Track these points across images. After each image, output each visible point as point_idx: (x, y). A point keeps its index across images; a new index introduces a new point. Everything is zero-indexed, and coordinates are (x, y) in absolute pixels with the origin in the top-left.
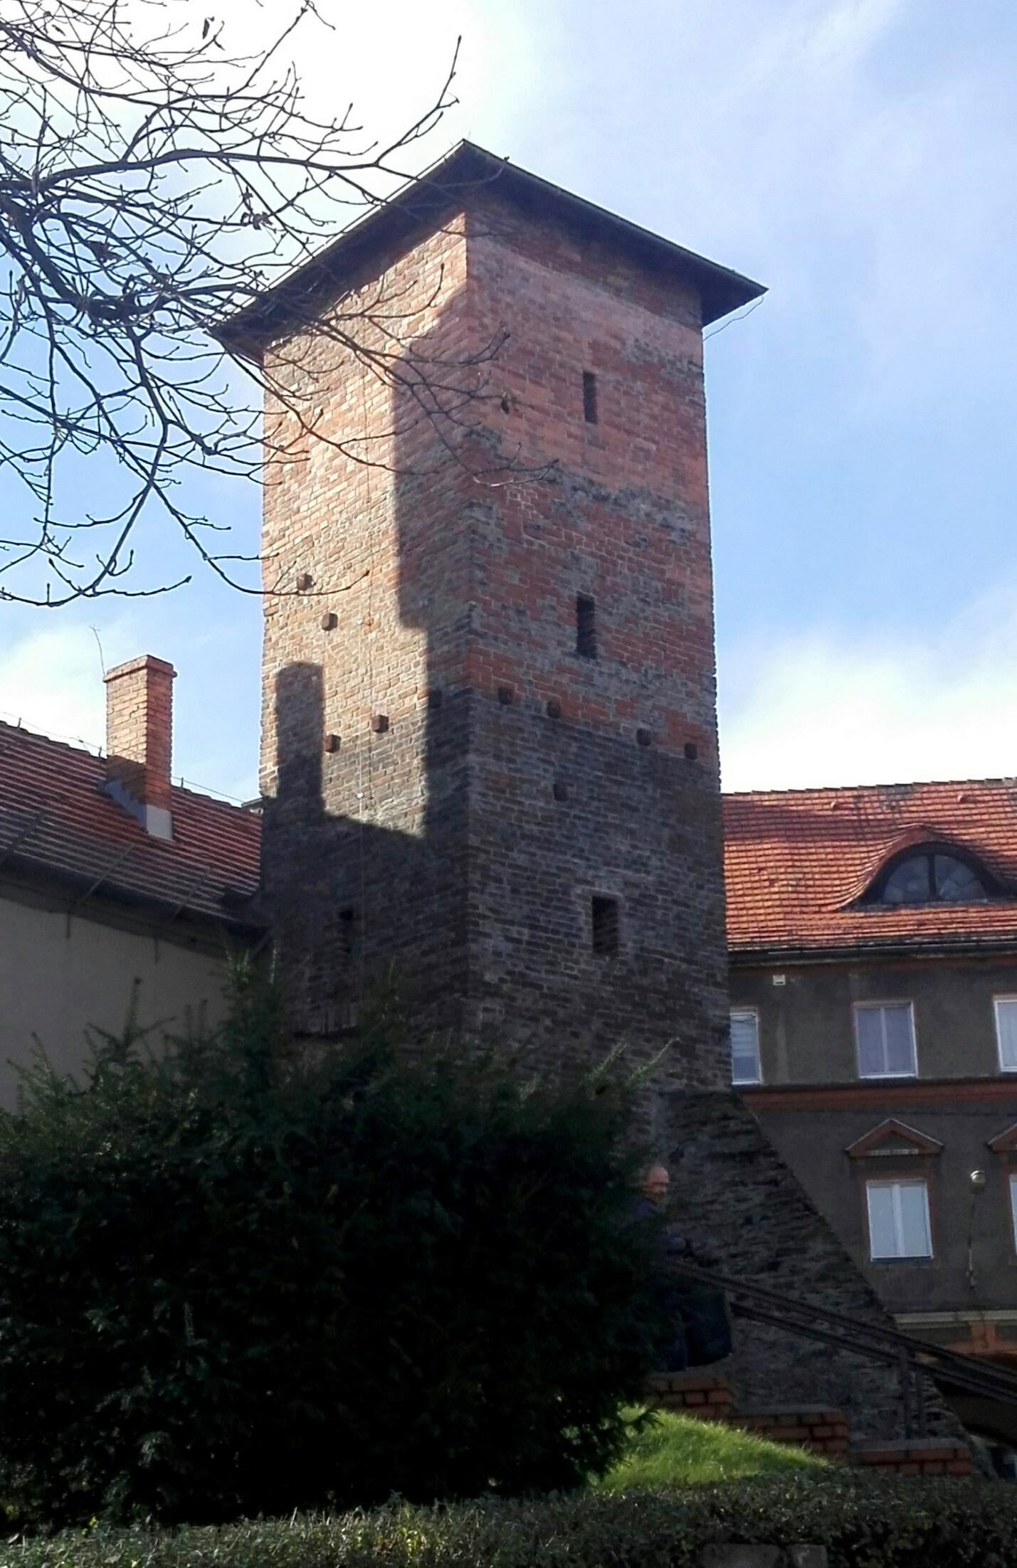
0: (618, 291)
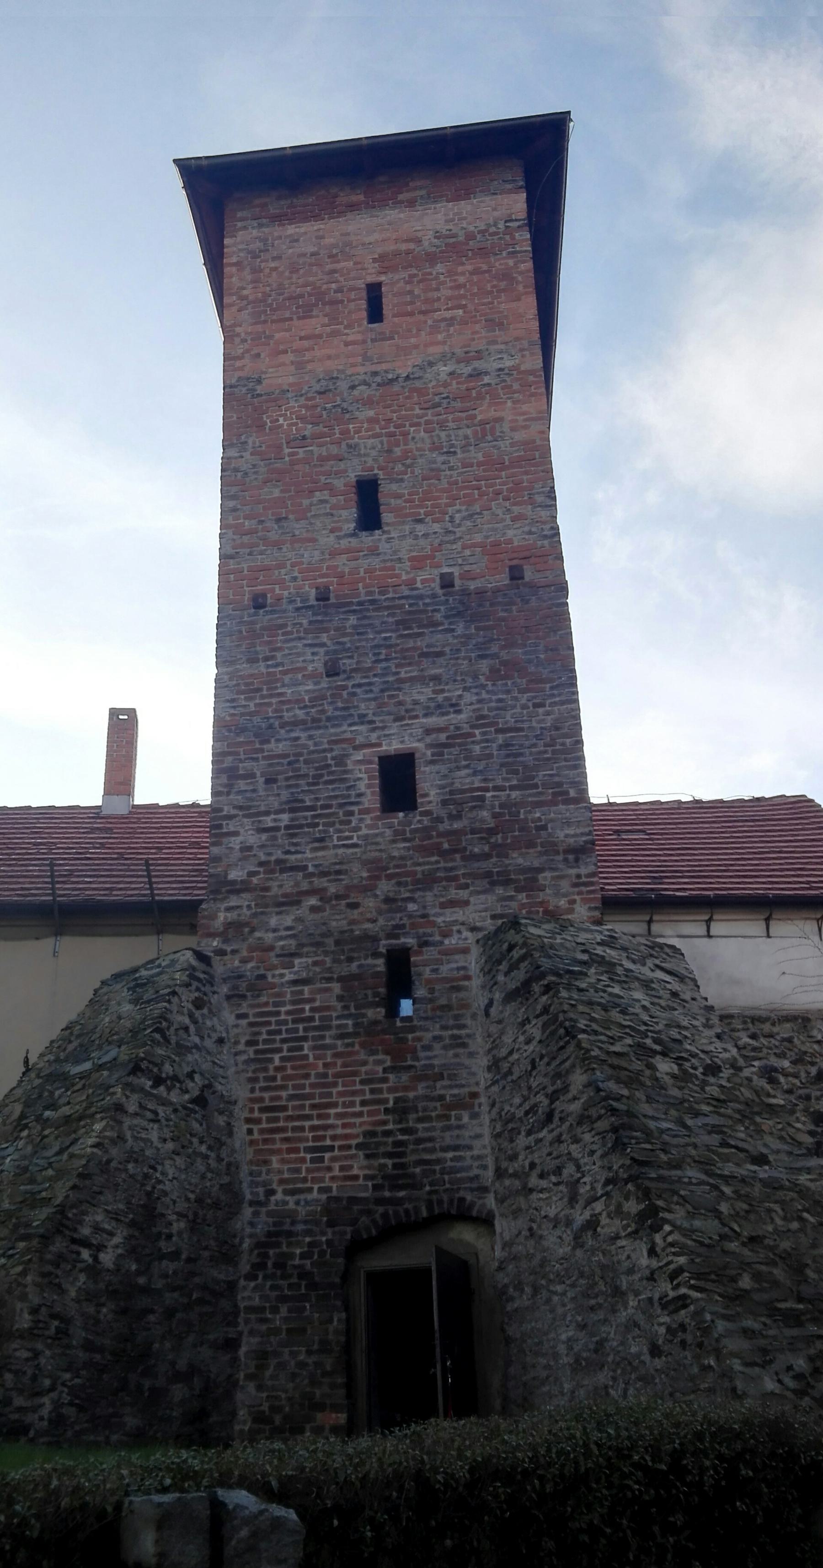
0: (411, 203)
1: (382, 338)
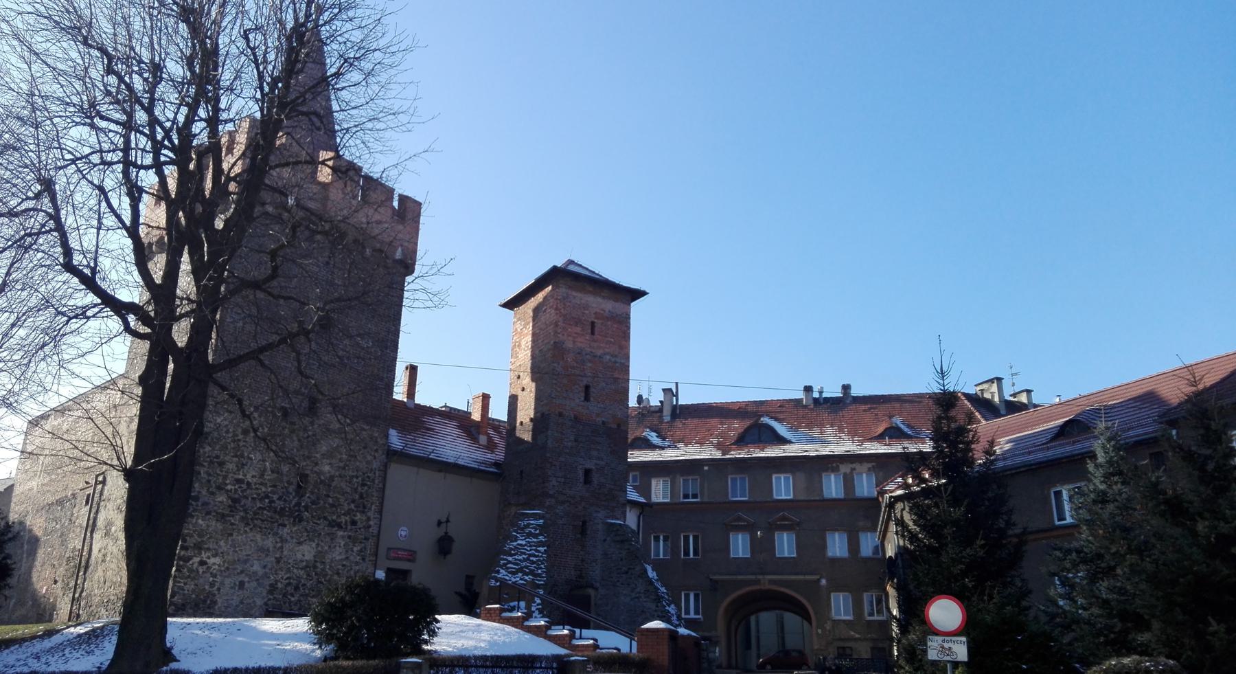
0: (604, 298)
1: (594, 341)
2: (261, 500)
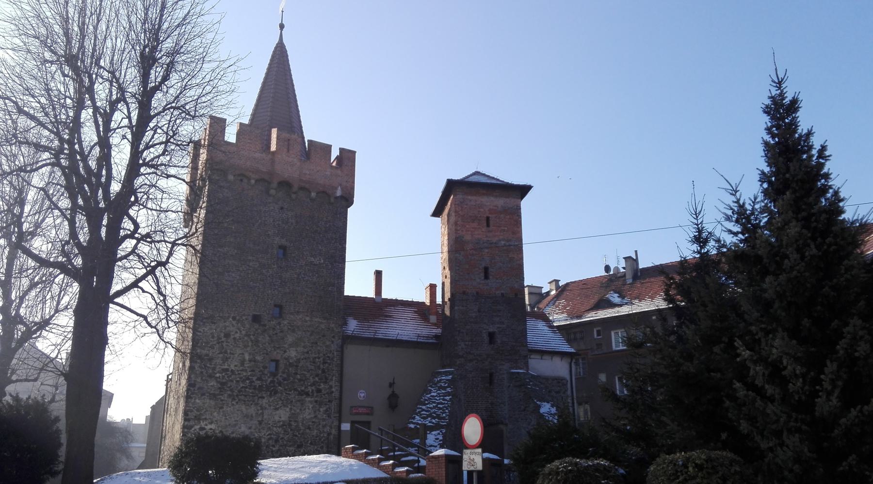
0: (496, 196)
1: (489, 231)
2: (244, 381)
